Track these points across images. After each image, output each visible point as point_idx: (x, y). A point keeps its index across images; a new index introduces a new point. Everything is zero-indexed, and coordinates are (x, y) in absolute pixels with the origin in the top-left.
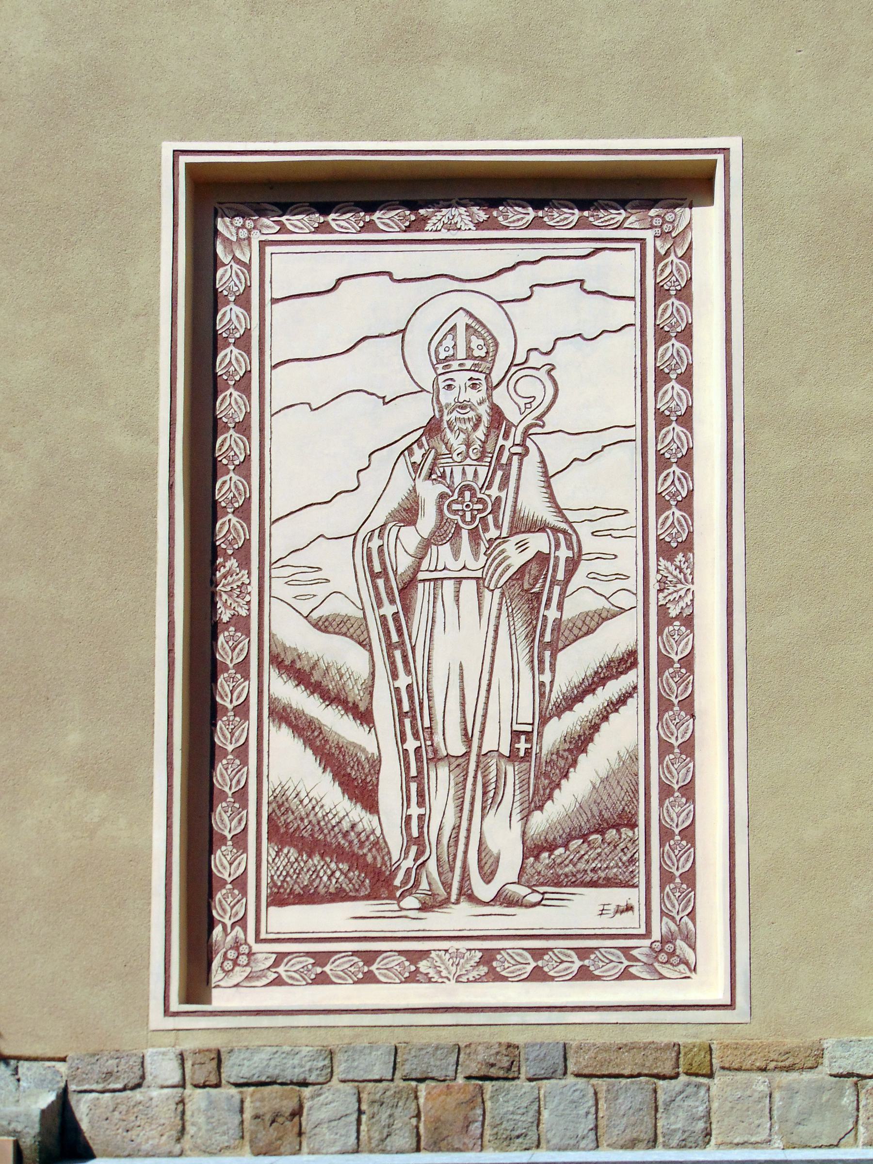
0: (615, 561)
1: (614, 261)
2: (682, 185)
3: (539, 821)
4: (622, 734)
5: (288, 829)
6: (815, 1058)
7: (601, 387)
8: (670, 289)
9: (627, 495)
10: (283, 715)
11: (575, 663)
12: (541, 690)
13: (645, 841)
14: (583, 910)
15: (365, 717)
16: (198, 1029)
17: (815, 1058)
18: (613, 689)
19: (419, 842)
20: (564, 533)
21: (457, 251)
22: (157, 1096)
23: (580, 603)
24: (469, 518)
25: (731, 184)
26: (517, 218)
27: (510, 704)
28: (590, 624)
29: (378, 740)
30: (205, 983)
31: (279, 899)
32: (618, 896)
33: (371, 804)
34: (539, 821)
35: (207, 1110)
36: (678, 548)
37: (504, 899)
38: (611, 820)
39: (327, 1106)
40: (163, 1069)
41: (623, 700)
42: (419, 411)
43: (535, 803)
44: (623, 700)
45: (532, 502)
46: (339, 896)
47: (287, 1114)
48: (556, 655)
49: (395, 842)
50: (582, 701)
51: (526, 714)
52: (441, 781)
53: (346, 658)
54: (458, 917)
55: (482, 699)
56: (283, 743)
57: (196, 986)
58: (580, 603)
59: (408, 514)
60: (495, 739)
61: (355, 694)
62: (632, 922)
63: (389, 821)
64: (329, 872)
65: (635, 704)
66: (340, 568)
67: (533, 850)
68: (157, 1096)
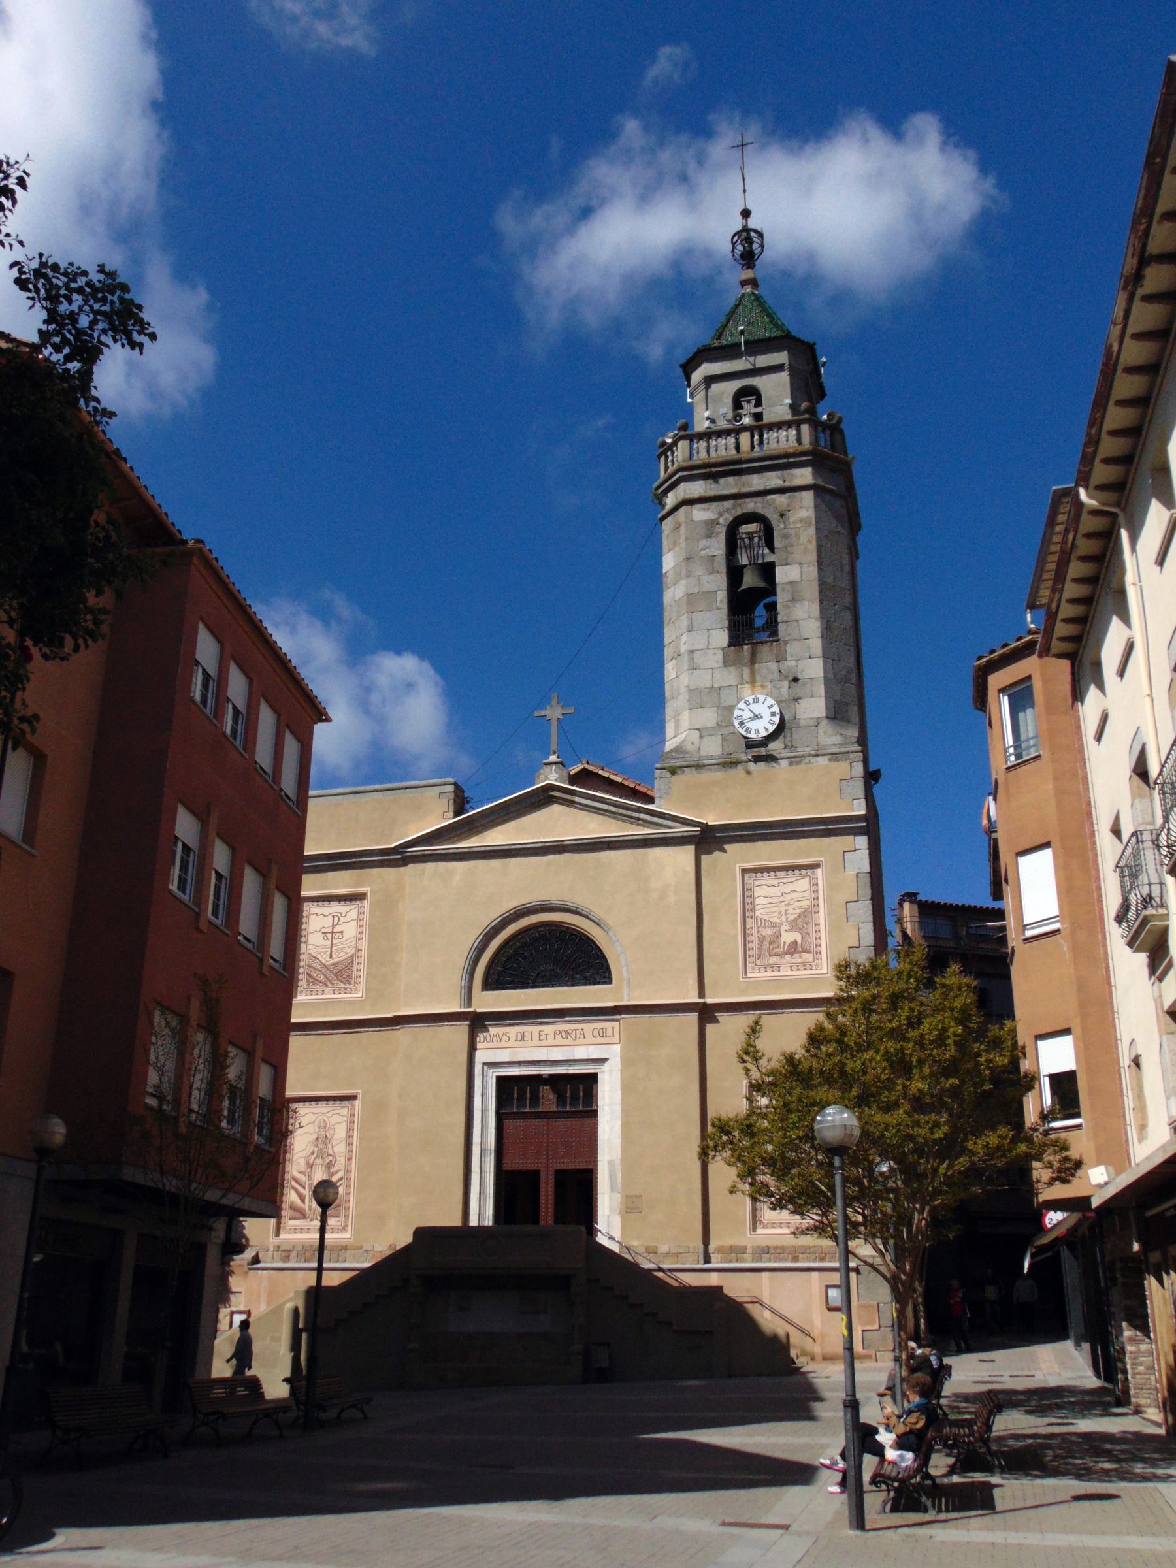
0: (341, 1160)
1: (343, 1109)
2: (352, 1098)
3: (180, 845)
5: (293, 1208)
6: (361, 1248)
7: (341, 1132)
8: (353, 1106)
9: (343, 1150)
10: (293, 1188)
16: (277, 1241)
17: (361, 1248)
20: (334, 1157)
21: (322, 1108)
22: (270, 1253)
23: (336, 1168)
24: (321, 1154)
25: (360, 1097)
26: (331, 1103)
28: (337, 1172)
31: (291, 1219)
34: (180, 845)
35: (1029, 1157)
36: (350, 1159)
39: (293, 1255)
40: (271, 1248)
42: (315, 1136)
45: (330, 1152)
47: (1039, 1122)
53: (302, 1178)
57: (277, 1234)
58: (336, 1168)
59: (313, 1153)
64: (297, 1214)
66: (302, 1162)
68: (270, 1253)
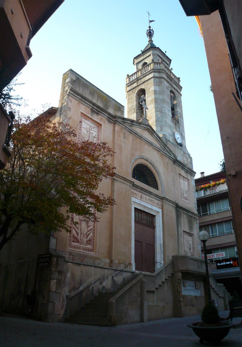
3: (87, 239)
4: (91, 234)
10: (74, 228)
11: (89, 228)
12: (87, 230)
13: (92, 242)
14: (89, 246)
15: (78, 229)
18: (91, 231)
19: (80, 239)
27: (86, 231)
29: (79, 231)
30: (180, 95)
32: (91, 246)
33: (78, 236)
37: (85, 245)
38: (90, 240)
41: (91, 232)
43: (87, 238)
44: (91, 232)
46: (76, 242)
48: (179, 85)
49: (79, 239)
50: (179, 79)
51: (87, 232)
52: (82, 235)
54: (82, 245)
55: (145, 139)
56: (74, 230)
60: (85, 233)
61: (78, 228)
62: (91, 248)
63: (79, 237)
64: (76, 240)
65: (92, 232)
67: (86, 241)
